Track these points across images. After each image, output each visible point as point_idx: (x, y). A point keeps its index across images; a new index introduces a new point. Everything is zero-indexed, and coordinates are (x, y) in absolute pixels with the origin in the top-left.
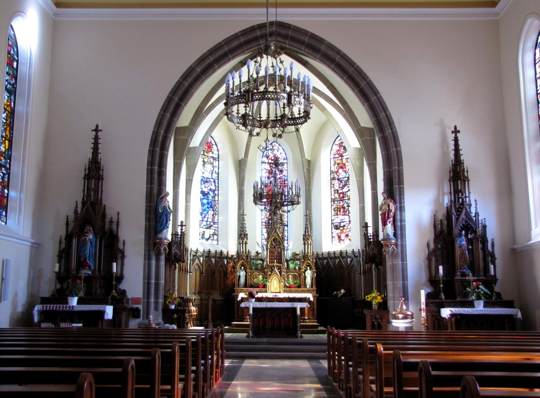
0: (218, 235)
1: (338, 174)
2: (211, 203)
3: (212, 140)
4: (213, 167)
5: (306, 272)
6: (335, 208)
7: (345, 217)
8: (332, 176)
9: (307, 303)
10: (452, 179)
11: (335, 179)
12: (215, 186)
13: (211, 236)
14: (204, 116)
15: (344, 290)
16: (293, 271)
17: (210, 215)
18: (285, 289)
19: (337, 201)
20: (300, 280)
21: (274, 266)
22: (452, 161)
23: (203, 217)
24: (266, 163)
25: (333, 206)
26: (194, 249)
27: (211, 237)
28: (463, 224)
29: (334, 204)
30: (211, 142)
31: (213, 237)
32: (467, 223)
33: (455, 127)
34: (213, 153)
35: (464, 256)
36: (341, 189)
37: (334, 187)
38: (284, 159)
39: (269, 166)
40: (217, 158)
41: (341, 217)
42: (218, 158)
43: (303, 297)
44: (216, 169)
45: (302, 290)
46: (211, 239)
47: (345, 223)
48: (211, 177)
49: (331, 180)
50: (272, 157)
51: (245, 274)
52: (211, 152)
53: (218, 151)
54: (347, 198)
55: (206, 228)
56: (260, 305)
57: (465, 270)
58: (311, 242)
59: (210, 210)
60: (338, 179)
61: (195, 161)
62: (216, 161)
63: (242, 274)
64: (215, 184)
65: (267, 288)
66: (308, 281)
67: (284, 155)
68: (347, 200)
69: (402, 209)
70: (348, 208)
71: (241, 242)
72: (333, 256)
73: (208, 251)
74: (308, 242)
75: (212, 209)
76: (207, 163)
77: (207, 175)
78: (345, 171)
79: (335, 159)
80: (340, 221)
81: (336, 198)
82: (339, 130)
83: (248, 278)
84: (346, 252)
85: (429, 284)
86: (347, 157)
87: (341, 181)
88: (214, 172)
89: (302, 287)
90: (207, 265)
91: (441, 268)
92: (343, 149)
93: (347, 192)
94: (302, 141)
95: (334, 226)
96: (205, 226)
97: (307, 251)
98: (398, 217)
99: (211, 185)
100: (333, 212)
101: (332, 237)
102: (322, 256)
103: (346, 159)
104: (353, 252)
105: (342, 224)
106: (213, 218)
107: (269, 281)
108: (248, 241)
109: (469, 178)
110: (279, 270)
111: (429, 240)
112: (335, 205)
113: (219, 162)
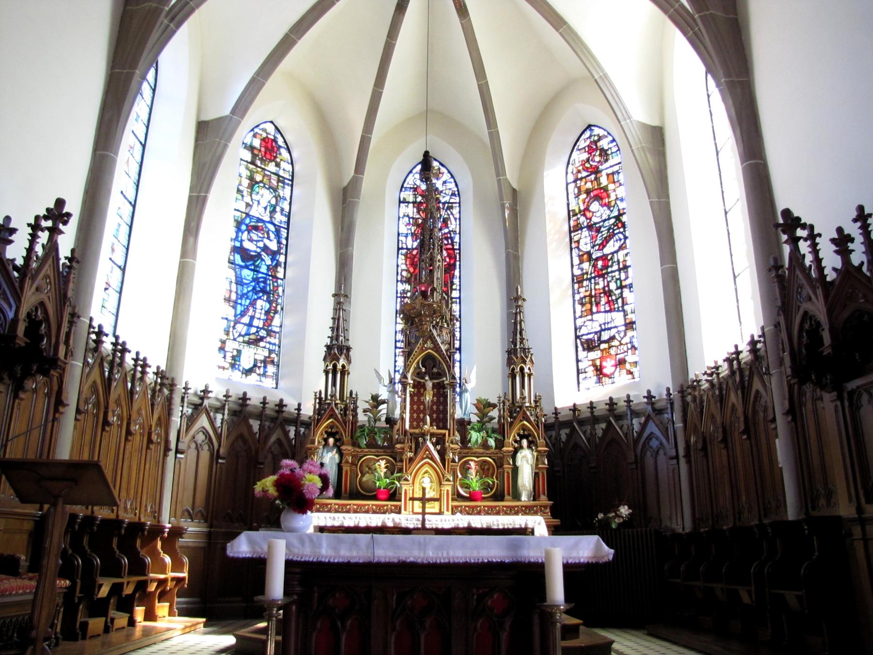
0: (278, 366)
1: (589, 215)
2: (265, 282)
3: (279, 136)
5: (519, 456)
6: (585, 297)
7: (614, 315)
8: (572, 223)
9: (596, 537)
11: (581, 229)
12: (279, 242)
13: (259, 365)
15: (629, 508)
16: (481, 451)
17: (258, 311)
18: (456, 503)
19: (590, 280)
20: (500, 477)
21: (423, 435)
23: (238, 312)
24: (409, 203)
25: (579, 293)
26: (196, 386)
27: (259, 367)
29: (579, 287)
30: (275, 140)
31: (265, 367)
34: (278, 165)
36: (599, 250)
37: (578, 248)
38: (453, 194)
39: (415, 210)
40: (289, 180)
41: (600, 318)
42: (292, 180)
44: (285, 205)
45: (507, 507)
46: (258, 371)
47: (613, 332)
48: (267, 219)
49: (570, 232)
51: (337, 461)
52: (274, 163)
53: (292, 164)
54: (615, 267)
55: (244, 342)
56: (335, 549)
58: (529, 369)
59: (260, 298)
60: (590, 227)
62: (286, 186)
65: (400, 500)
66: (526, 479)
67: (452, 186)
68: (617, 273)
70: (622, 293)
71: (330, 367)
72: (589, 415)
73: (241, 396)
74: (522, 369)
75: (265, 298)
76: (262, 185)
78: (608, 205)
79: (578, 182)
80: (599, 329)
81: (587, 273)
82: (600, 77)
83: (347, 472)
84: (629, 401)
86: (610, 171)
87: (598, 231)
88: (278, 209)
89: (507, 497)
90: (233, 437)
92: (600, 155)
93: (616, 252)
95: (582, 344)
96: (243, 336)
97: (522, 393)
99: (268, 238)
100: (578, 308)
101: (578, 373)
102: (556, 418)
103: (608, 175)
104: (649, 396)
105: (605, 336)
106: (266, 320)
107: (406, 480)
108: (351, 368)
110: (439, 447)
112: (582, 290)
113: (292, 190)
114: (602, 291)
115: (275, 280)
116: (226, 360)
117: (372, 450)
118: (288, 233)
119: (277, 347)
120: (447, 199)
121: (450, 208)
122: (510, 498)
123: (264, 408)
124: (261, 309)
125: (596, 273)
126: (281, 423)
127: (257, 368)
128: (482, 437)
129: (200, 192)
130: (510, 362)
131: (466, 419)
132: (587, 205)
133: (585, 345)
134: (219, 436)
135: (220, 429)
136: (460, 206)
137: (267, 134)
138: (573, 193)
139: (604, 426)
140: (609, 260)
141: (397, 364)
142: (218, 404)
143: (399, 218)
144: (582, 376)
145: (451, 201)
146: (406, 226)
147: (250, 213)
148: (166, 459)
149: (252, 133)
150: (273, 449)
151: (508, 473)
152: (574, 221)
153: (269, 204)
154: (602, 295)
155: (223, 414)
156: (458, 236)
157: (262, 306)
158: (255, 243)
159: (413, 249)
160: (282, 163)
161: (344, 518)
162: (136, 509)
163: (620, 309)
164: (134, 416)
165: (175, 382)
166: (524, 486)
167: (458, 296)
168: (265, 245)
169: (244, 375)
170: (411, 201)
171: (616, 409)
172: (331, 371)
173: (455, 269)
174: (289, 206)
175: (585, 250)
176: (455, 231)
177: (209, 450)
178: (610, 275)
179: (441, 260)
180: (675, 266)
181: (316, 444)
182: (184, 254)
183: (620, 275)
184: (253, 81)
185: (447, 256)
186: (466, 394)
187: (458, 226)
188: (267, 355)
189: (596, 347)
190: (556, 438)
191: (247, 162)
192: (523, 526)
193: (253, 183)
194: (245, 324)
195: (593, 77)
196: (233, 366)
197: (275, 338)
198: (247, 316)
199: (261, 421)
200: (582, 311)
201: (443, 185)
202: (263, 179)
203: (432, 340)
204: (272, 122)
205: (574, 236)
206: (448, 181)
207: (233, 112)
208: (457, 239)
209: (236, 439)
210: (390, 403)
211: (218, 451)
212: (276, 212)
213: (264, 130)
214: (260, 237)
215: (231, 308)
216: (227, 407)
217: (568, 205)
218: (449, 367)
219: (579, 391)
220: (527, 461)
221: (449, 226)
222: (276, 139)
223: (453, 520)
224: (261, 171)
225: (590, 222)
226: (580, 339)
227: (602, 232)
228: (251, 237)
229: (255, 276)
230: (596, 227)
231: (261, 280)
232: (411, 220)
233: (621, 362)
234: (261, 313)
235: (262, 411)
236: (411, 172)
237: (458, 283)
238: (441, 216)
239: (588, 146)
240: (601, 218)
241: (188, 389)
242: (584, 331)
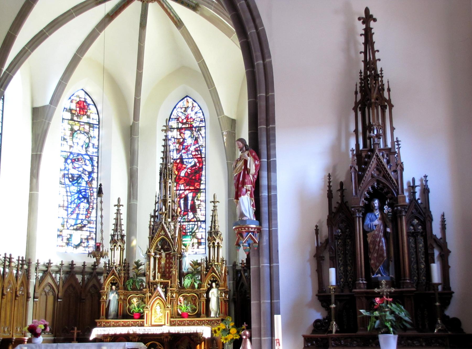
2: (85, 192)
3: (87, 97)
4: (89, 138)
10: (360, 106)
12: (93, 166)
13: (84, 241)
14: (27, 50)
16: (190, 290)
17: (81, 210)
22: (361, 73)
23: (69, 212)
24: (174, 128)
26: (43, 261)
27: (84, 243)
28: (373, 187)
30: (85, 101)
31: (88, 242)
32: (381, 186)
33: (367, 10)
34: (88, 117)
35: (377, 247)
38: (201, 121)
39: (178, 133)
42: (99, 124)
43: (192, 332)
44: (95, 141)
50: (183, 120)
52: (86, 116)
53: (98, 114)
55: (74, 229)
57: (380, 275)
59: (82, 202)
61: (43, 127)
63: (113, 297)
64: (92, 163)
65: (144, 319)
66: (213, 305)
67: (200, 115)
69: (271, 167)
73: (71, 263)
74: (214, 243)
76: (79, 132)
77: (77, 149)
85: (318, 304)
88: (91, 145)
89: (202, 315)
90: (66, 287)
91: (332, 271)
94: (215, 88)
96: (73, 226)
98: (264, 182)
107: (147, 308)
109: (393, 102)
111: (320, 222)
115: (91, 189)
116: (63, 241)
117: (135, 292)
121: (199, 130)
122: (205, 315)
124: (84, 209)
126: (95, 275)
127: (83, 243)
128: (191, 282)
129: (37, 152)
131: (185, 272)
134: (58, 287)
135: (59, 283)
136: (205, 129)
137: (80, 98)
142: (57, 269)
145: (200, 126)
147: (73, 152)
148: (28, 303)
149: (70, 100)
150: (91, 291)
151: (203, 302)
153: (84, 143)
155: (60, 274)
156: (204, 149)
157: (84, 206)
158: (77, 169)
159: (177, 159)
160: (91, 115)
161: (110, 330)
162: (10, 331)
164: (6, 284)
165: (31, 261)
166: (212, 308)
167: (204, 188)
168: (83, 169)
169: (75, 248)
170: (176, 127)
173: (202, 170)
176: (203, 146)
177: (53, 295)
179: (171, 183)
181: (106, 290)
182: (31, 189)
184: (60, 83)
185: (198, 162)
187: (204, 142)
188: (89, 235)
191: (68, 120)
192: (195, 332)
193: (73, 132)
196: (68, 244)
198: (75, 214)
199: (83, 275)
202: (79, 129)
203: (164, 231)
204: (82, 89)
206: (198, 112)
207: (51, 102)
208: (203, 151)
209: (69, 286)
211: (58, 295)
213: (78, 96)
214: (80, 165)
215: (65, 211)
216: (62, 270)
220: (214, 295)
221: (199, 142)
222: (86, 100)
223: (161, 329)
224: (78, 123)
228: (74, 166)
229: (78, 190)
232: (176, 140)
235: (83, 270)
236: (175, 107)
237: (204, 180)
238: (194, 136)
241: (39, 263)
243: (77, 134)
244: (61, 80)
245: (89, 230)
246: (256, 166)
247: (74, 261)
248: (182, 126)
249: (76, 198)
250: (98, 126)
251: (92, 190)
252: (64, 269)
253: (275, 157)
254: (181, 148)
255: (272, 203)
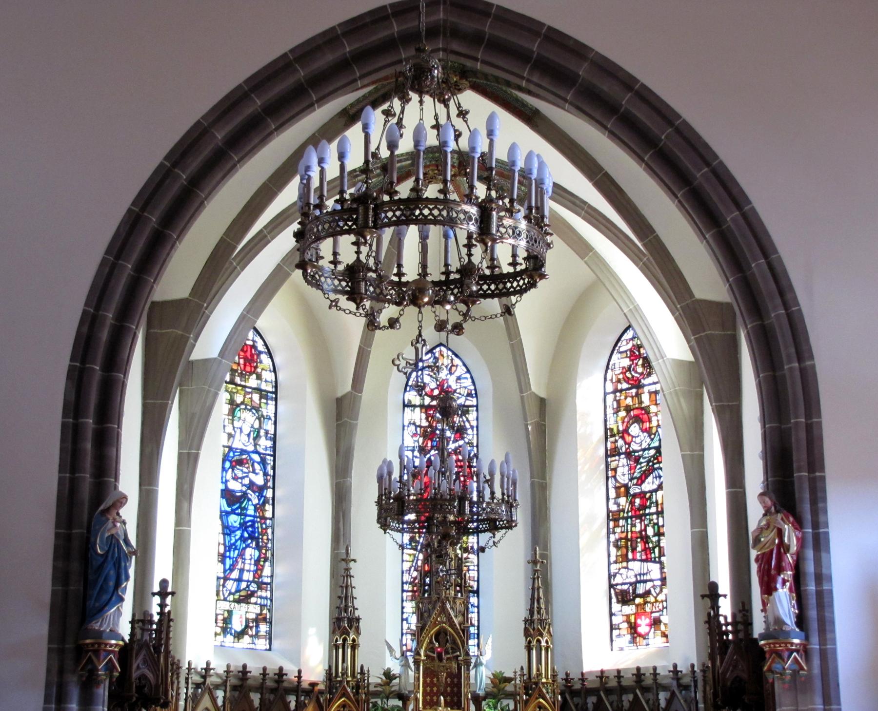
0: (271, 623)
1: (628, 439)
2: (253, 526)
3: (258, 339)
4: (259, 418)
6: (621, 539)
11: (619, 454)
12: (265, 474)
13: (251, 625)
17: (248, 562)
19: (626, 519)
23: (228, 567)
24: (415, 406)
25: (614, 533)
26: (200, 665)
27: (251, 628)
29: (615, 526)
30: (254, 347)
31: (257, 626)
34: (259, 377)
37: (614, 477)
38: (469, 395)
39: (424, 416)
41: (635, 566)
42: (276, 393)
44: (269, 426)
46: (250, 633)
47: (649, 585)
49: (607, 456)
50: (432, 390)
52: (254, 376)
53: (275, 371)
55: (235, 601)
58: (547, 642)
59: (248, 546)
60: (629, 455)
62: (270, 402)
64: (265, 468)
68: (655, 517)
69: (820, 543)
70: (659, 541)
71: (340, 642)
74: (539, 641)
76: (243, 407)
80: (633, 580)
81: (623, 511)
86: (653, 388)
87: (637, 460)
88: (262, 432)
92: (643, 366)
93: (656, 491)
96: (234, 594)
97: (538, 670)
98: (810, 567)
99: (254, 472)
100: (613, 551)
103: (650, 393)
104: (675, 671)
105: (641, 589)
108: (361, 640)
112: (618, 530)
113: (276, 405)
114: (638, 535)
115: (263, 521)
118: (274, 461)
119: (269, 601)
120: (461, 401)
123: (264, 679)
124: (251, 559)
125: (633, 512)
130: (527, 633)
132: (627, 426)
133: (620, 597)
136: (477, 410)
138: (611, 406)
139: (631, 697)
140: (647, 500)
141: (405, 610)
143: (404, 426)
144: (615, 633)
146: (412, 437)
147: (234, 446)
152: (612, 442)
154: (639, 540)
157: (251, 555)
158: (240, 480)
163: (657, 559)
169: (236, 639)
170: (418, 403)
171: (643, 681)
172: (341, 646)
174: (273, 426)
175: (623, 482)
176: (472, 443)
178: (648, 517)
180: (705, 530)
183: (658, 519)
186: (481, 668)
187: (475, 436)
188: (259, 612)
189: (630, 600)
190: (582, 707)
194: (235, 580)
195: (623, 311)
197: (266, 590)
200: (617, 556)
201: (457, 382)
205: (611, 461)
206: (463, 376)
207: (195, 290)
210: (403, 678)
212: (260, 437)
214: (245, 473)
217: (606, 421)
218: (463, 643)
219: (612, 650)
224: (242, 390)
225: (629, 448)
226: (615, 589)
227: (642, 463)
228: (235, 475)
230: (635, 456)
231: (248, 524)
232: (418, 429)
233: (656, 623)
234: (250, 564)
239: (631, 350)
240: (641, 446)
242: (618, 580)
243: (240, 410)
244: (245, 313)
245: (259, 602)
246: (798, 539)
247: (248, 665)
248: (432, 401)
249: (237, 537)
250: (274, 396)
251: (265, 523)
252: (233, 681)
253: (827, 527)
254: (429, 445)
255: (826, 604)
